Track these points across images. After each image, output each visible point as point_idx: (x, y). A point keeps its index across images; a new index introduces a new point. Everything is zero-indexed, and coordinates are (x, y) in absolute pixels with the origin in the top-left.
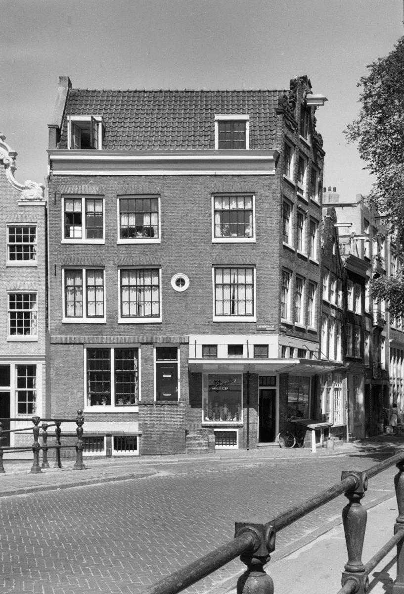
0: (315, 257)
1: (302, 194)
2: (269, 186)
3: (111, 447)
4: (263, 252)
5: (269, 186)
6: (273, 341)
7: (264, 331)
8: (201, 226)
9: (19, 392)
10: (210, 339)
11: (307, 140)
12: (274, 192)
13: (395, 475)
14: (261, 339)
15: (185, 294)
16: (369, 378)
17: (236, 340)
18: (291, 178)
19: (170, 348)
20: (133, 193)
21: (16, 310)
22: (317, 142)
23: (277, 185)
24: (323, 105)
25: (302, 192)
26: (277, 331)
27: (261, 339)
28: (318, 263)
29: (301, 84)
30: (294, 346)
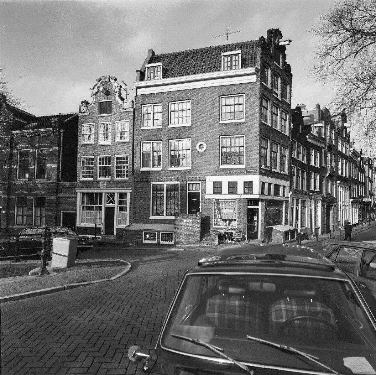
0: (287, 133)
1: (277, 96)
2: (253, 89)
3: (159, 239)
4: (250, 127)
5: (253, 89)
6: (256, 179)
7: (249, 173)
8: (213, 114)
9: (120, 207)
10: (218, 179)
11: (280, 66)
12: (256, 92)
13: (350, 368)
14: (248, 178)
15: (204, 153)
16: (218, 299)
17: (233, 178)
18: (269, 86)
19: (279, 185)
20: (177, 100)
21: (102, 165)
22: (288, 68)
23: (257, 88)
24: (289, 44)
25: (277, 95)
26: (258, 173)
27: (248, 178)
28: (289, 136)
29: (275, 33)
30: (271, 183)
